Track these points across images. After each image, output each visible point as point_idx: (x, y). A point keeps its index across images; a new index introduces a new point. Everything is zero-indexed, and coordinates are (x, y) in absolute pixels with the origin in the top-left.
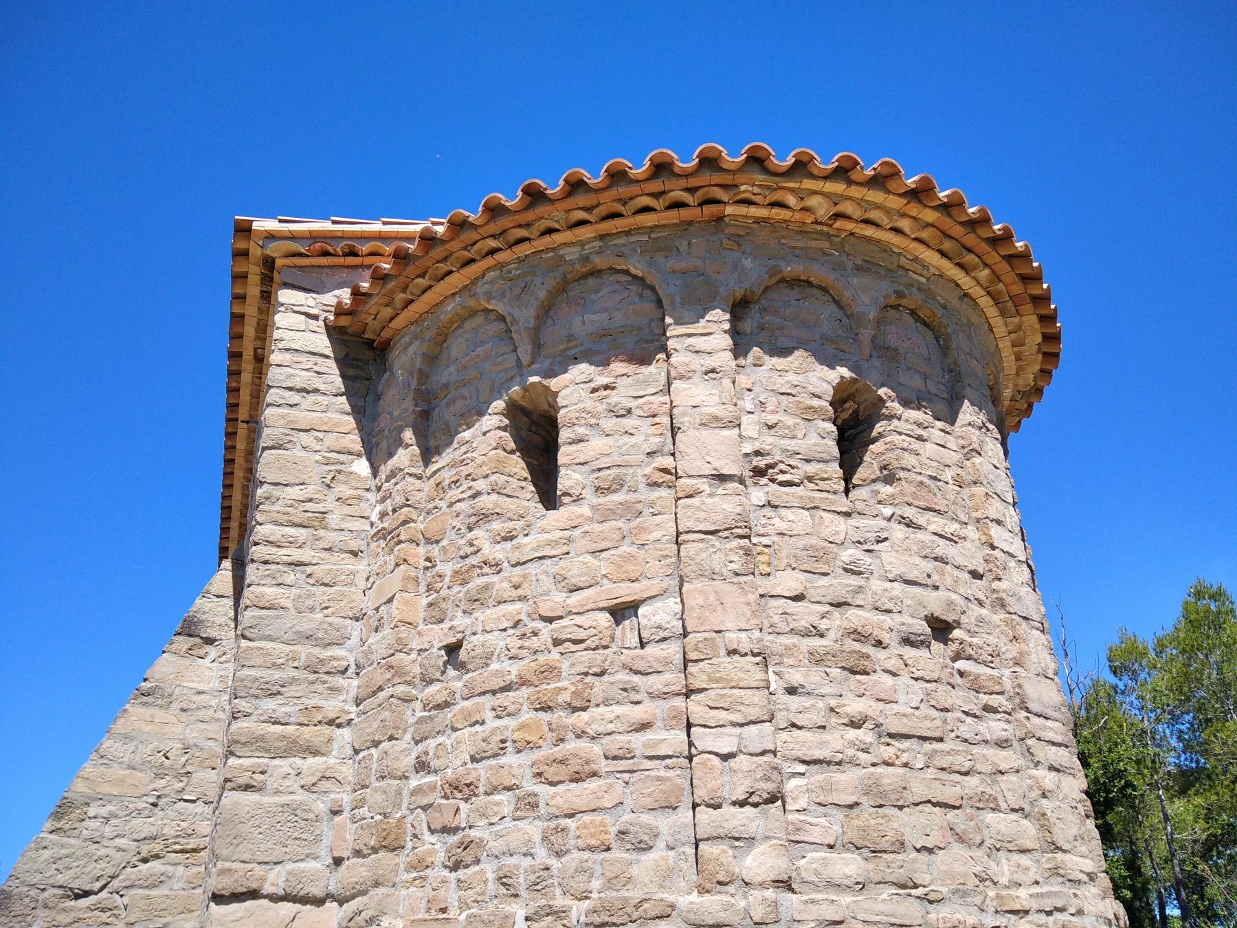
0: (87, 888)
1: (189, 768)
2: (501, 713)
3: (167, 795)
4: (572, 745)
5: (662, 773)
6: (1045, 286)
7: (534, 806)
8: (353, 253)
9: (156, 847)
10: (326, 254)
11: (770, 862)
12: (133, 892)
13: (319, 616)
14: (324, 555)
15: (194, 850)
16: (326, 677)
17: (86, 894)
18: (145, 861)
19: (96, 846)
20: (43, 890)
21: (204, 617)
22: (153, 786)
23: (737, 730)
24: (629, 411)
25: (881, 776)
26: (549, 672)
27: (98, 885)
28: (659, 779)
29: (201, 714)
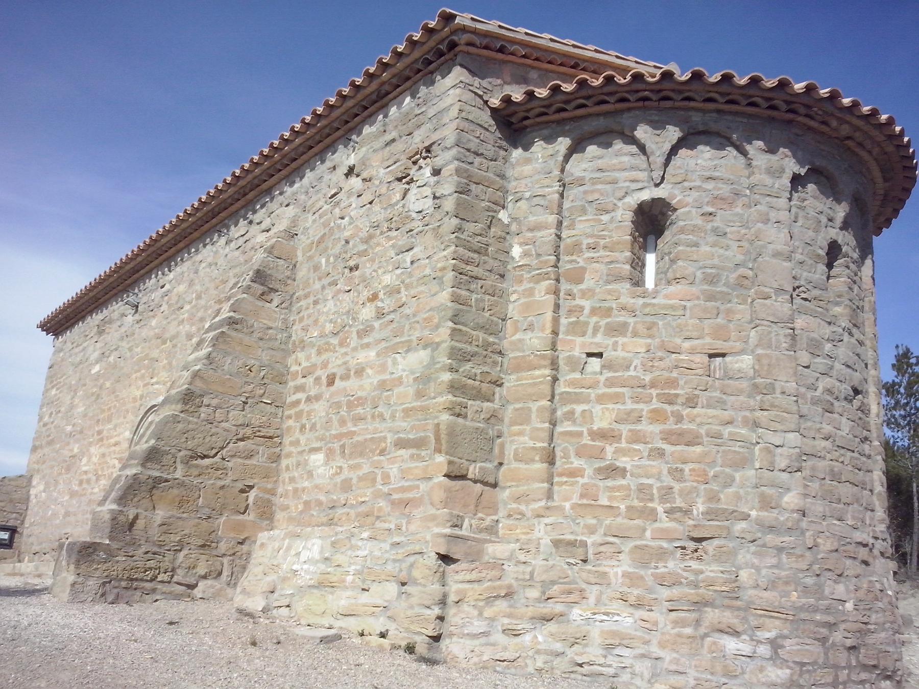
0: (206, 453)
1: (265, 381)
2: (637, 399)
3: (253, 397)
4: (685, 426)
5: (737, 449)
6: (911, 150)
7: (664, 454)
8: (501, 50)
9: (248, 431)
10: (486, 47)
11: (796, 501)
12: (234, 460)
13: (487, 314)
14: (487, 274)
15: (271, 437)
16: (491, 355)
17: (205, 457)
18: (242, 440)
19: (210, 426)
20: (180, 451)
21: (269, 272)
22: (243, 390)
23: (783, 434)
24: (725, 234)
25: (834, 466)
26: (673, 383)
27: (214, 451)
28: (735, 452)
29: (271, 344)
